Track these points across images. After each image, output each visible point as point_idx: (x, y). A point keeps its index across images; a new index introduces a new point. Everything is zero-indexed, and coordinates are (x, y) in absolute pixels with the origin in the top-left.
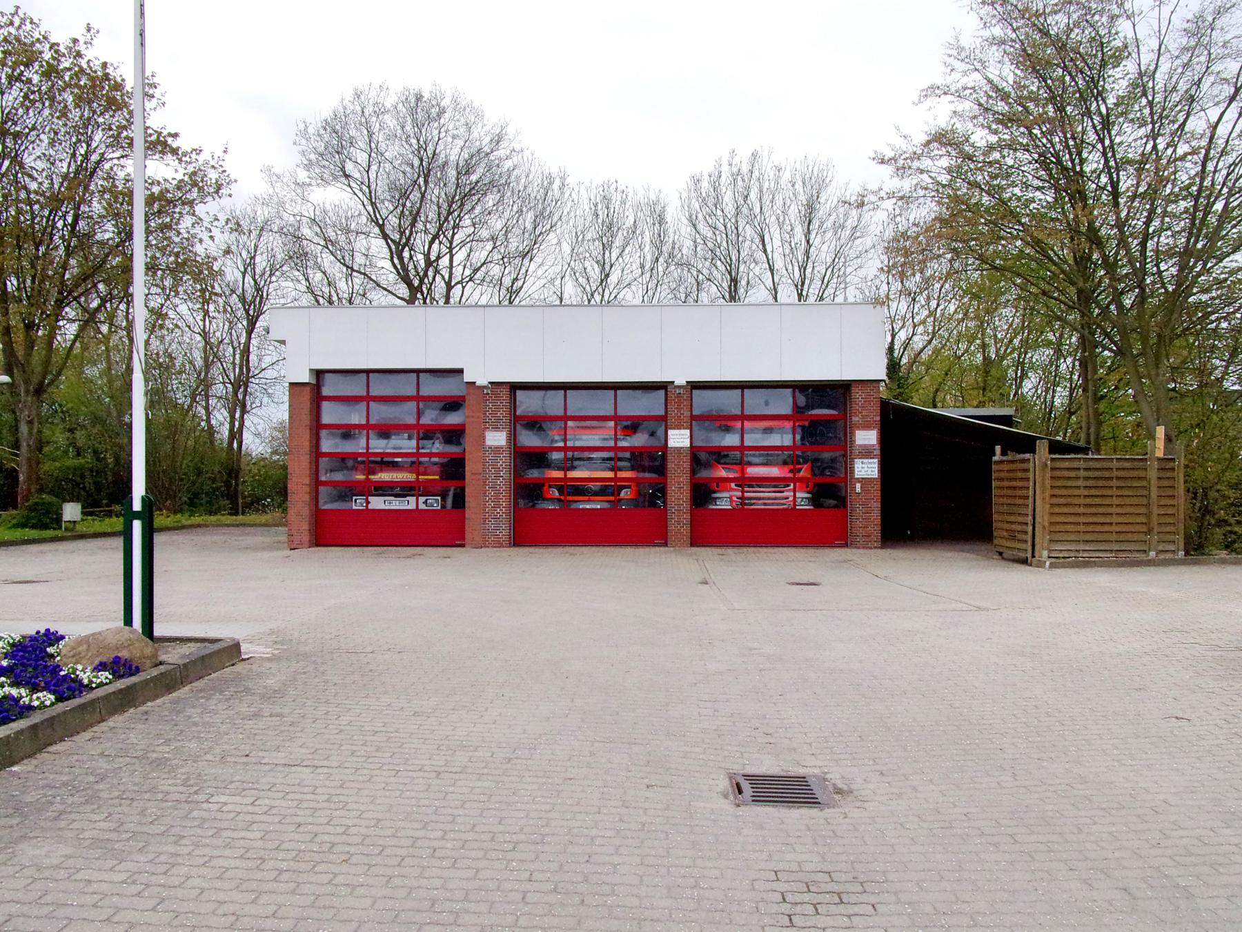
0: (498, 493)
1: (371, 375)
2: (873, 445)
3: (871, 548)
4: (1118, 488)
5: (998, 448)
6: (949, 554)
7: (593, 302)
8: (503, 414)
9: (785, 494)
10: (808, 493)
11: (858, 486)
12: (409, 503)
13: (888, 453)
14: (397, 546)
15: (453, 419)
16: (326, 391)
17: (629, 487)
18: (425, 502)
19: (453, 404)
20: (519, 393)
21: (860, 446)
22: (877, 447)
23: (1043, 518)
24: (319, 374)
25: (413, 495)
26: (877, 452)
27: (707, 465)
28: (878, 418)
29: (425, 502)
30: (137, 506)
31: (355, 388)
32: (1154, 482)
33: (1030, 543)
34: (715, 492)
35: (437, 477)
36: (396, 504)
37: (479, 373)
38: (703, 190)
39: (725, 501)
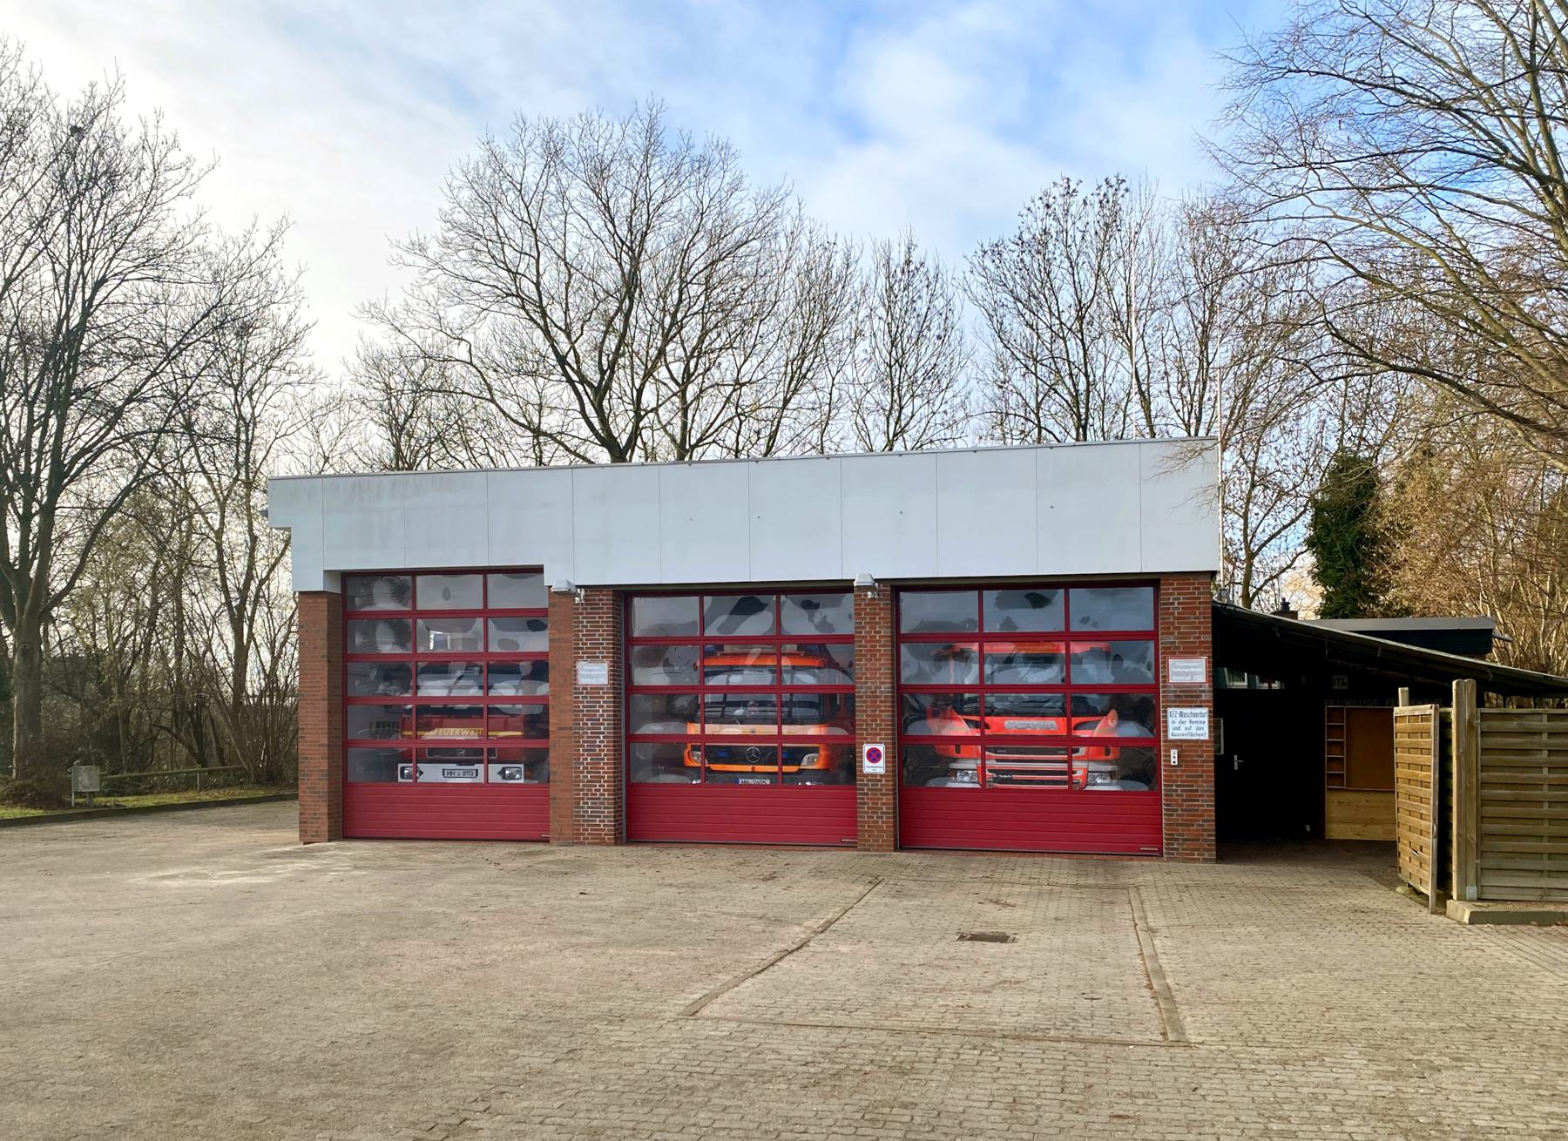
0: (597, 760)
1: (490, 577)
2: (1201, 684)
3: (1197, 860)
7: (898, 446)
8: (604, 636)
10: (1107, 762)
11: (1174, 753)
13: (1224, 705)
15: (535, 643)
17: (815, 750)
19: (535, 621)
20: (905, 597)
21: (1177, 685)
22: (1207, 687)
24: (346, 577)
25: (481, 762)
27: (922, 714)
28: (1209, 638)
29: (502, 773)
31: (468, 596)
34: (955, 760)
35: (519, 733)
36: (461, 777)
38: (834, 270)
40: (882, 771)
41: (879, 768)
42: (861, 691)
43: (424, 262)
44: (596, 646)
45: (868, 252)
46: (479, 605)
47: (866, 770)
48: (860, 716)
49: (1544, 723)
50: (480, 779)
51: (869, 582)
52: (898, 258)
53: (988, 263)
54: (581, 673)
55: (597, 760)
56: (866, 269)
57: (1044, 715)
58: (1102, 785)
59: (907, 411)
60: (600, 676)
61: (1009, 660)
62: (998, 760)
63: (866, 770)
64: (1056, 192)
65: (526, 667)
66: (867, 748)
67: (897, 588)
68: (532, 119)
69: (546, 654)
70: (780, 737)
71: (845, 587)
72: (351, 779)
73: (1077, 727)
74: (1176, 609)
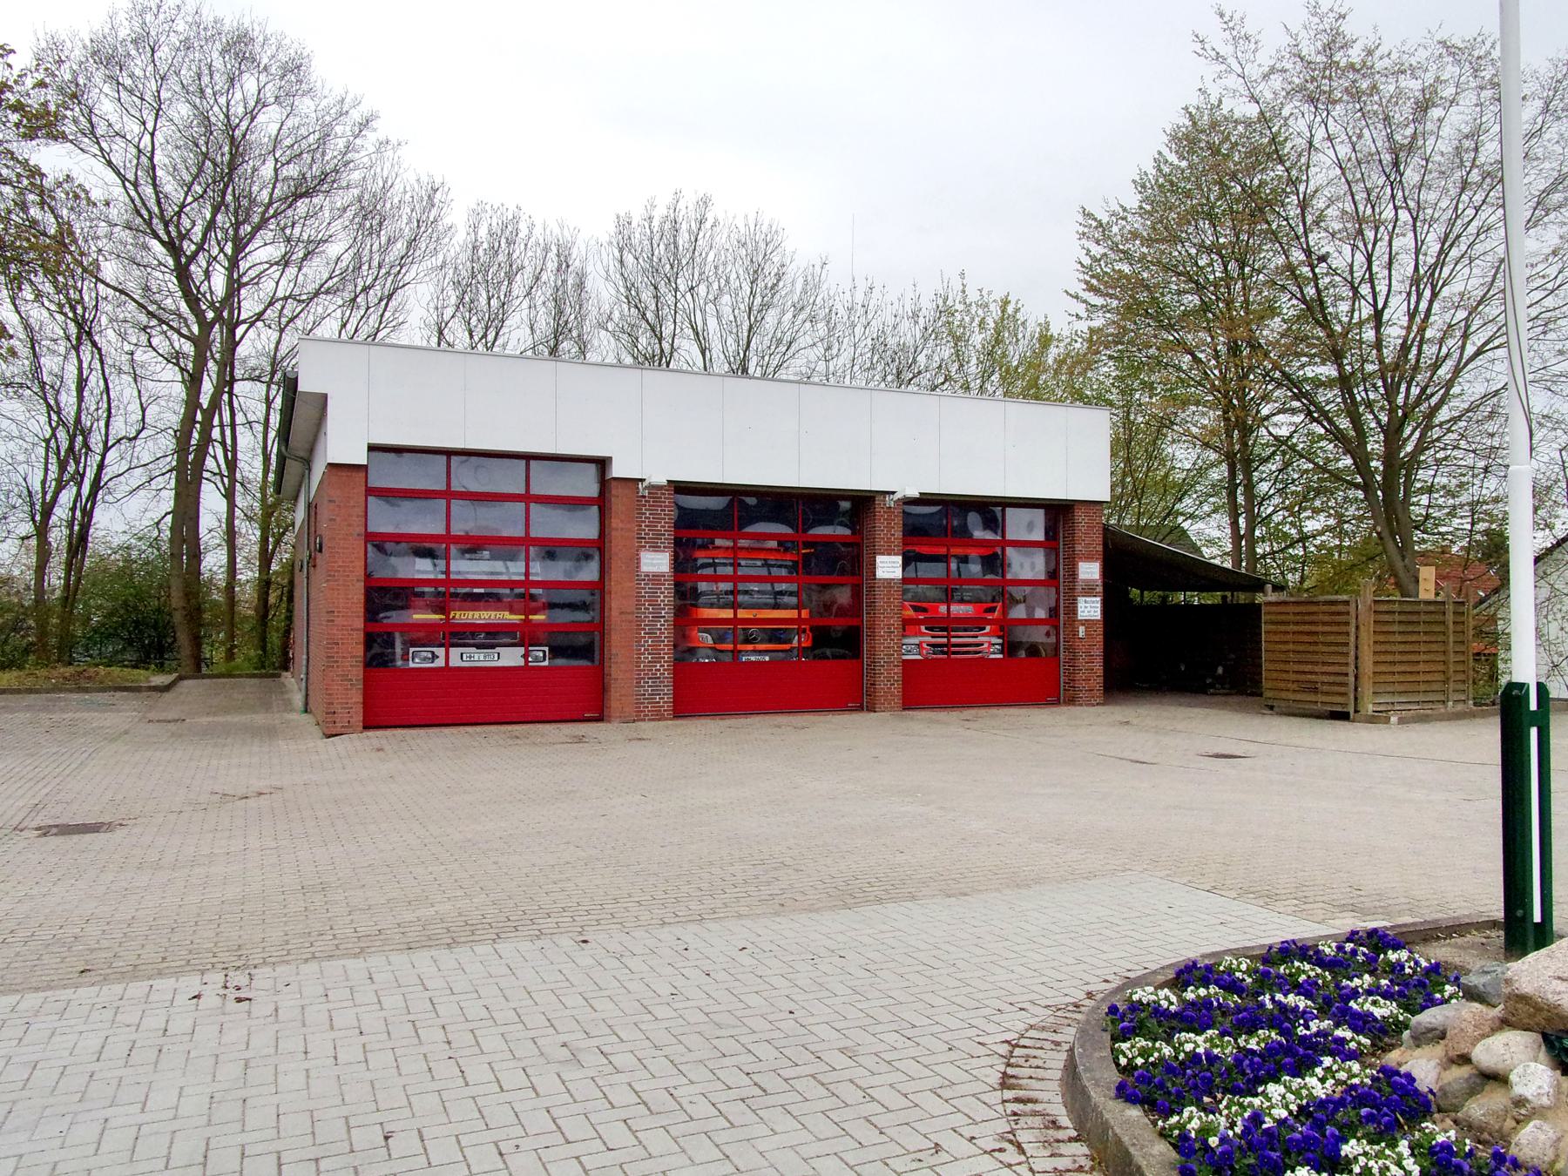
0: (658, 640)
1: (533, 463)
4: (1425, 633)
9: (980, 639)
10: (999, 637)
12: (511, 657)
14: (396, 727)
18: (434, 657)
21: (1084, 581)
22: (1100, 583)
23: (1367, 664)
26: (1100, 589)
29: (434, 657)
32: (1451, 625)
44: (659, 535)
50: (440, 663)
60: (659, 564)
62: (933, 637)
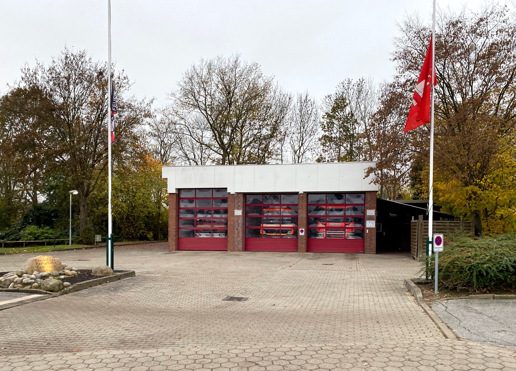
0: (239, 232)
2: (373, 215)
5: (413, 217)
6: (134, 253)
8: (241, 204)
11: (367, 230)
13: (379, 219)
15: (224, 205)
16: (182, 196)
17: (291, 230)
20: (309, 195)
22: (375, 216)
24: (179, 190)
26: (375, 218)
28: (376, 205)
30: (110, 237)
31: (191, 195)
33: (416, 252)
34: (318, 232)
37: (232, 190)
39: (322, 235)
40: (304, 235)
41: (303, 234)
42: (299, 217)
43: (175, 99)
44: (239, 206)
45: (296, 96)
46: (211, 197)
47: (300, 235)
48: (299, 222)
49: (448, 224)
51: (302, 193)
52: (304, 98)
53: (327, 101)
54: (235, 212)
55: (239, 232)
56: (295, 101)
57: (339, 222)
58: (351, 238)
59: (305, 139)
61: (332, 210)
63: (300, 235)
64: (346, 82)
65: (222, 211)
66: (300, 229)
67: (308, 194)
68: (205, 59)
69: (227, 208)
70: (280, 227)
71: (297, 193)
72: (179, 237)
73: (347, 225)
74: (369, 199)
